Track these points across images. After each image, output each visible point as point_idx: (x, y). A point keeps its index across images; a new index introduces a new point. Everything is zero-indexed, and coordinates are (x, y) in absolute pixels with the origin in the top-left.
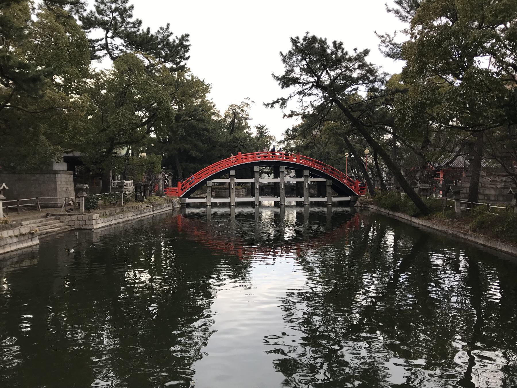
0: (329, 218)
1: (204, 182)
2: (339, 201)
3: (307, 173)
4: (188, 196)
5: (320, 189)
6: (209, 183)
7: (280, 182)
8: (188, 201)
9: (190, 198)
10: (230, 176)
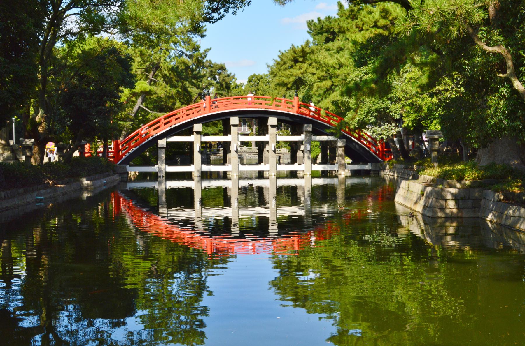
7: (267, 142)
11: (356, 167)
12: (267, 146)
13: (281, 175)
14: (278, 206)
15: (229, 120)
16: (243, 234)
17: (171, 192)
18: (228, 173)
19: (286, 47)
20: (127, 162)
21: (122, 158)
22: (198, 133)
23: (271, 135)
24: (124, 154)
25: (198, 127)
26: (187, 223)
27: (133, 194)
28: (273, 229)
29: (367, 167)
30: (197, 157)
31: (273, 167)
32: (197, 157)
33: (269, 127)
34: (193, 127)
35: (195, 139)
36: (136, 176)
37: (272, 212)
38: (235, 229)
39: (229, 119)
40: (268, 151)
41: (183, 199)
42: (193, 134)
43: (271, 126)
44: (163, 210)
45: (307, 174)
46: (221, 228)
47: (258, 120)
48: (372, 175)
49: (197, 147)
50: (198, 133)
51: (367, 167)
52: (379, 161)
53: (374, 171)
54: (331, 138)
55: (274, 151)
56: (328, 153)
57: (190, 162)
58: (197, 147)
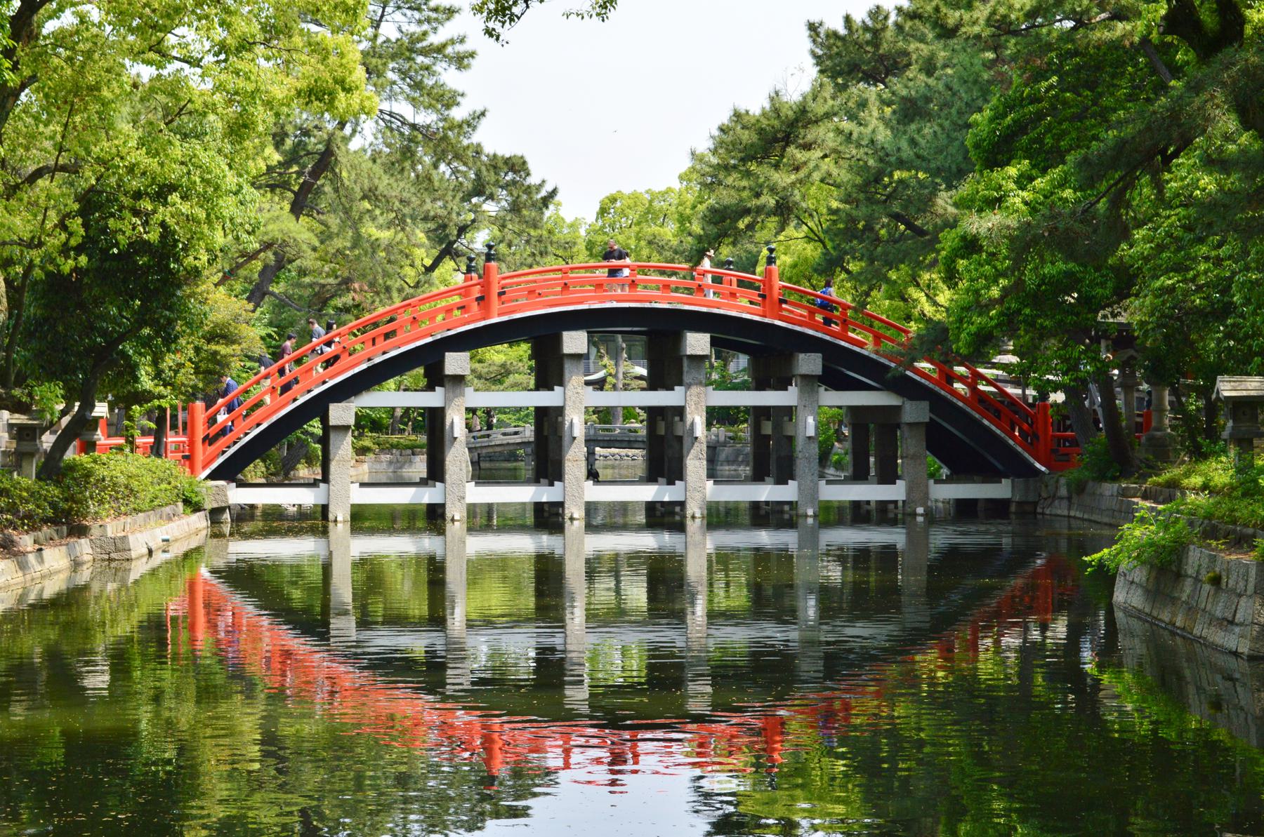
0: (908, 579)
1: (318, 407)
2: (854, 410)
3: (810, 363)
4: (230, 471)
5: (870, 445)
6: (341, 413)
8: (238, 496)
9: (241, 484)
10: (436, 378)
25: (455, 363)
29: (1000, 490)
47: (658, 339)
51: (1000, 490)
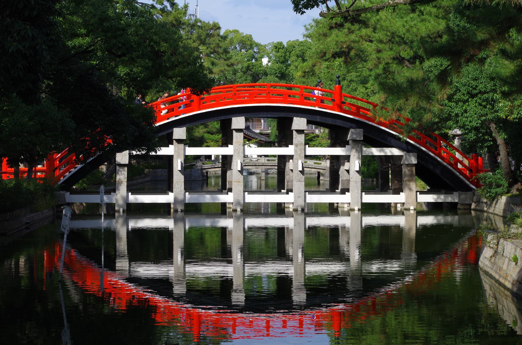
7: (291, 157)
11: (431, 198)
12: (347, 164)
13: (319, 211)
14: (307, 258)
15: (230, 122)
16: (257, 303)
17: (136, 235)
18: (228, 206)
19: (245, 31)
20: (67, 186)
21: (59, 180)
22: (179, 141)
23: (296, 146)
24: (63, 175)
25: (180, 133)
26: (163, 286)
27: (77, 238)
28: (299, 296)
30: (178, 179)
31: (299, 197)
32: (178, 179)
33: (294, 132)
34: (172, 132)
35: (175, 151)
36: (82, 208)
37: (300, 268)
38: (238, 298)
39: (230, 121)
40: (348, 171)
41: (152, 246)
42: (172, 144)
43: (176, 140)
44: (122, 264)
45: (350, 207)
46: (218, 293)
48: (459, 212)
49: (178, 165)
50: (179, 141)
52: (471, 189)
53: (462, 204)
54: (395, 152)
55: (302, 172)
56: (380, 176)
57: (168, 188)
58: (178, 165)
